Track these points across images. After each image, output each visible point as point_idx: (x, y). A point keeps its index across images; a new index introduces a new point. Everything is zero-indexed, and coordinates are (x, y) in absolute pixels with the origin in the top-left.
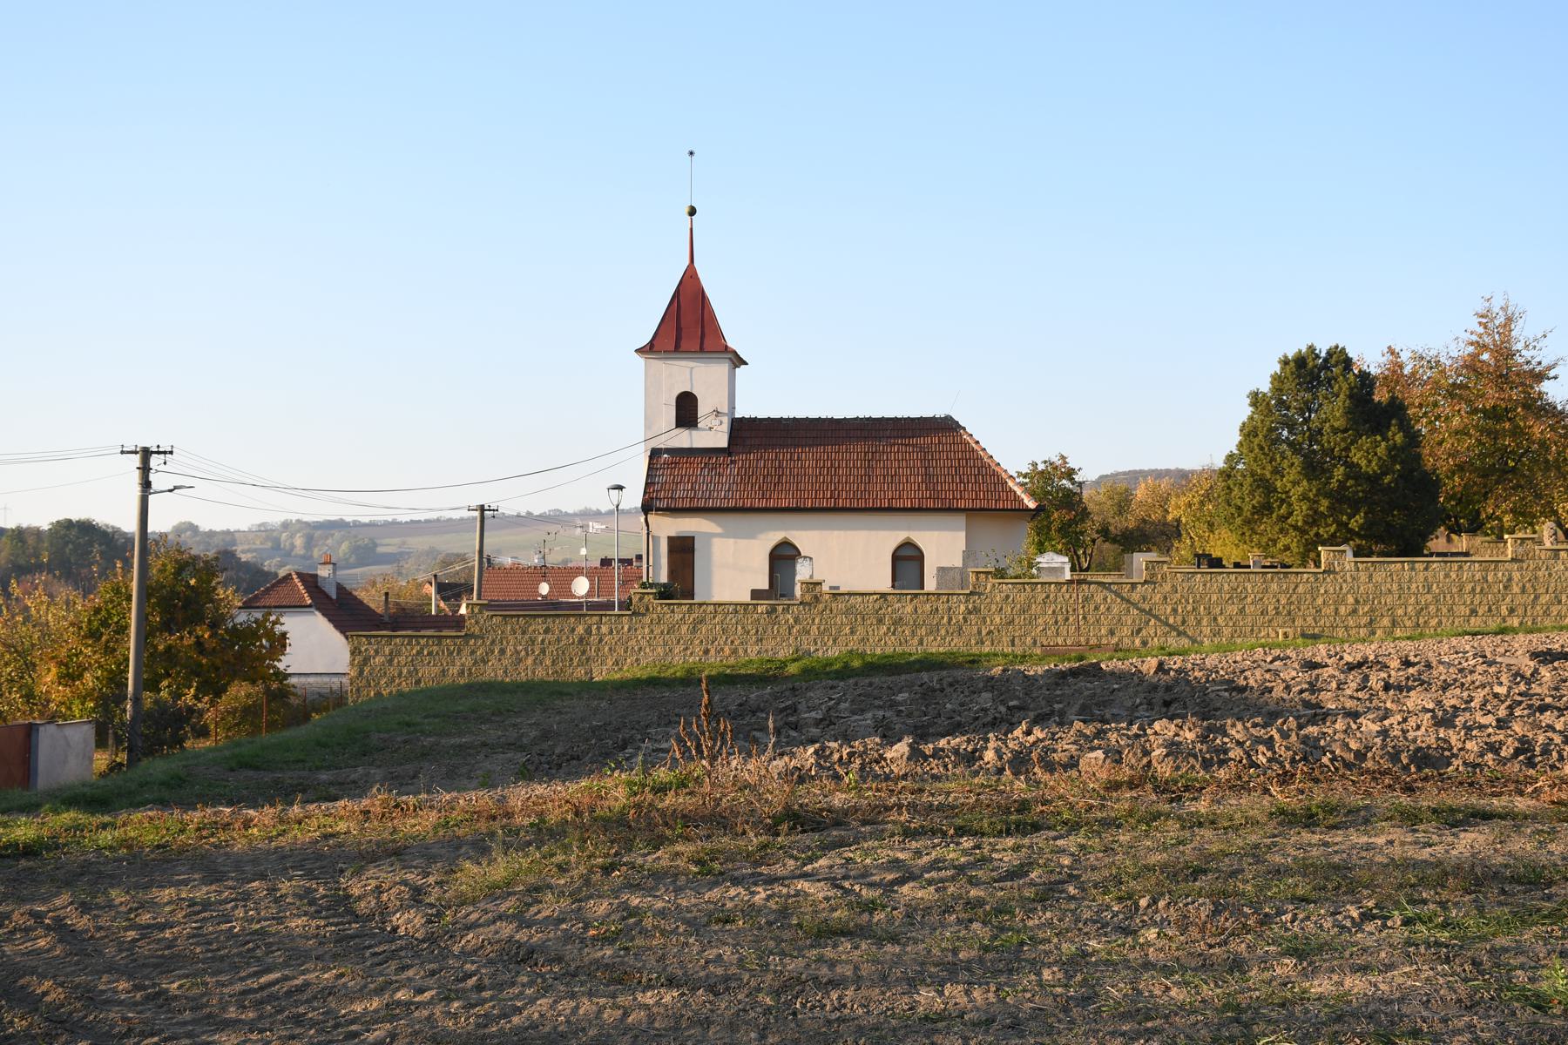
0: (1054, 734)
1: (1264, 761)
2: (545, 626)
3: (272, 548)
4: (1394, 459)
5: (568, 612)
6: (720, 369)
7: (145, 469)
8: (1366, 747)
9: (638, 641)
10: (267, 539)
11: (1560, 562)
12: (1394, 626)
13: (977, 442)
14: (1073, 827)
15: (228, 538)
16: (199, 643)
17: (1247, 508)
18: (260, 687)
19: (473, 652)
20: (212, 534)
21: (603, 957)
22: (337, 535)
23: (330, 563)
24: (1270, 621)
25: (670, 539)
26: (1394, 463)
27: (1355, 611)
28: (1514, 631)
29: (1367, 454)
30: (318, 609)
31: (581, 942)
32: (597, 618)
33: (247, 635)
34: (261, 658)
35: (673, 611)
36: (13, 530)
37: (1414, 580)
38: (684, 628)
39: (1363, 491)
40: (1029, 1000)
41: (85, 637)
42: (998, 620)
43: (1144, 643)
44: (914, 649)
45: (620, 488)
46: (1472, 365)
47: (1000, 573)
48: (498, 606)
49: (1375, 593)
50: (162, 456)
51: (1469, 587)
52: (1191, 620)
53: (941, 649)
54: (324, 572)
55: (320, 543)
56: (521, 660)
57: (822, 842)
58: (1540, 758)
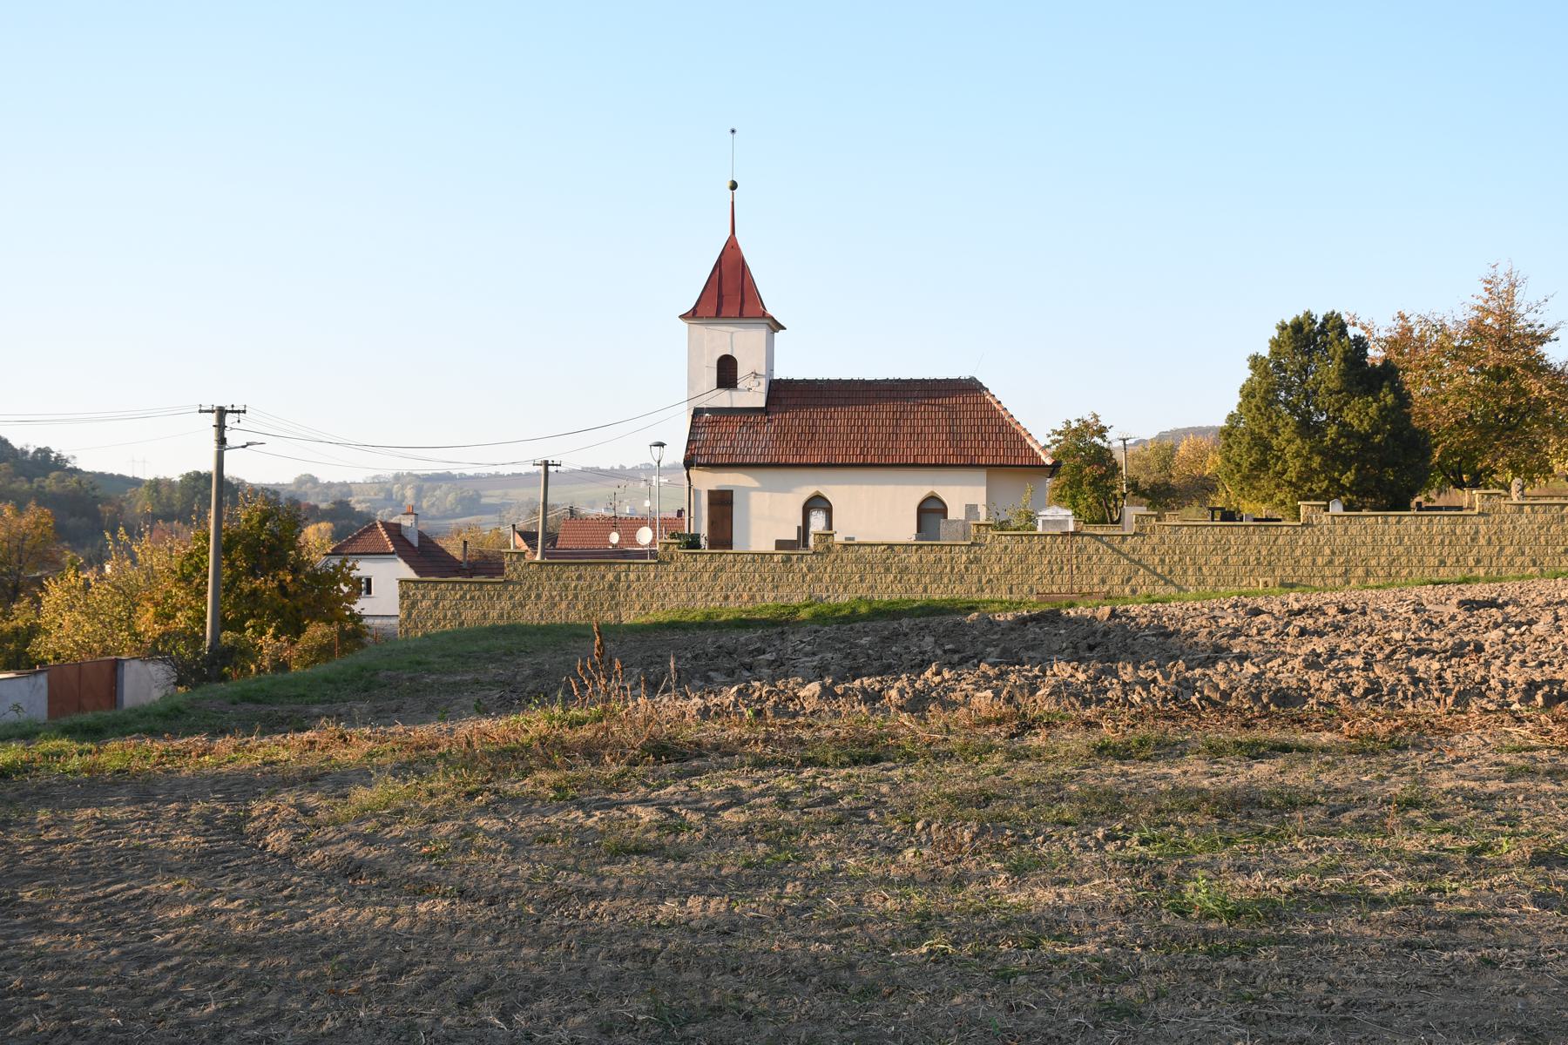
0: (960, 675)
1: (1138, 700)
2: (577, 573)
3: (385, 499)
4: (1384, 419)
5: (590, 561)
6: (758, 334)
7: (221, 427)
8: (1231, 688)
9: (663, 588)
10: (381, 490)
11: (1524, 516)
12: (1367, 575)
13: (999, 402)
14: (911, 758)
15: (345, 490)
16: (282, 587)
17: (1245, 464)
18: (335, 628)
19: (511, 597)
20: (330, 485)
21: (416, 872)
22: (445, 487)
23: (412, 513)
24: (1251, 571)
25: (711, 493)
26: (1385, 422)
27: (1331, 562)
28: (1477, 580)
29: (1360, 415)
30: (400, 556)
31: (407, 858)
32: (626, 566)
33: (327, 579)
34: (338, 601)
35: (695, 560)
36: (151, 481)
37: (1386, 533)
38: (706, 576)
39: (1355, 449)
40: (754, 910)
41: (179, 580)
42: (997, 569)
43: (1134, 591)
44: (919, 596)
45: (661, 445)
46: (1477, 330)
47: (1003, 526)
48: (571, 554)
49: (1350, 545)
50: (236, 415)
51: (1438, 539)
52: (1178, 570)
53: (944, 596)
54: (407, 522)
55: (429, 494)
56: (555, 605)
57: (677, 771)
58: (1386, 698)
